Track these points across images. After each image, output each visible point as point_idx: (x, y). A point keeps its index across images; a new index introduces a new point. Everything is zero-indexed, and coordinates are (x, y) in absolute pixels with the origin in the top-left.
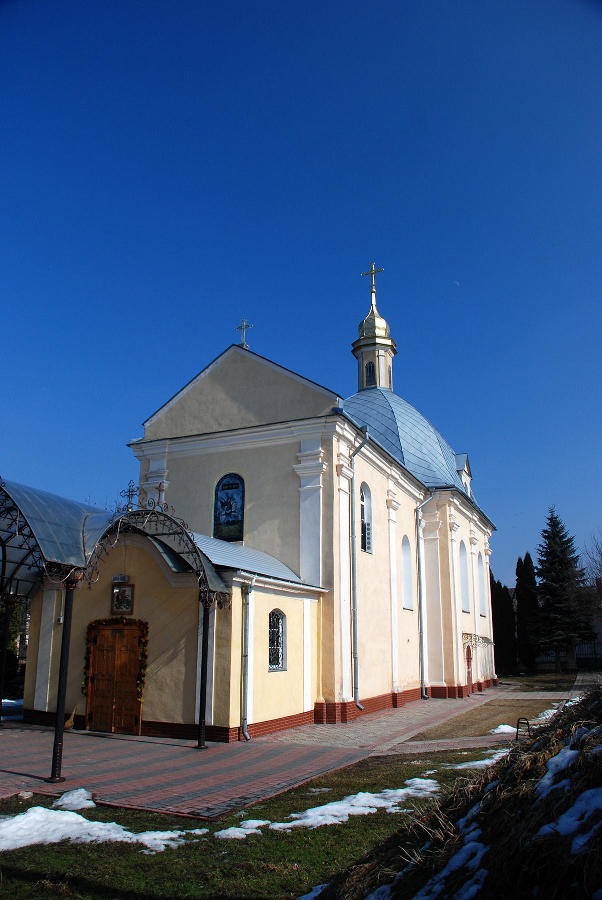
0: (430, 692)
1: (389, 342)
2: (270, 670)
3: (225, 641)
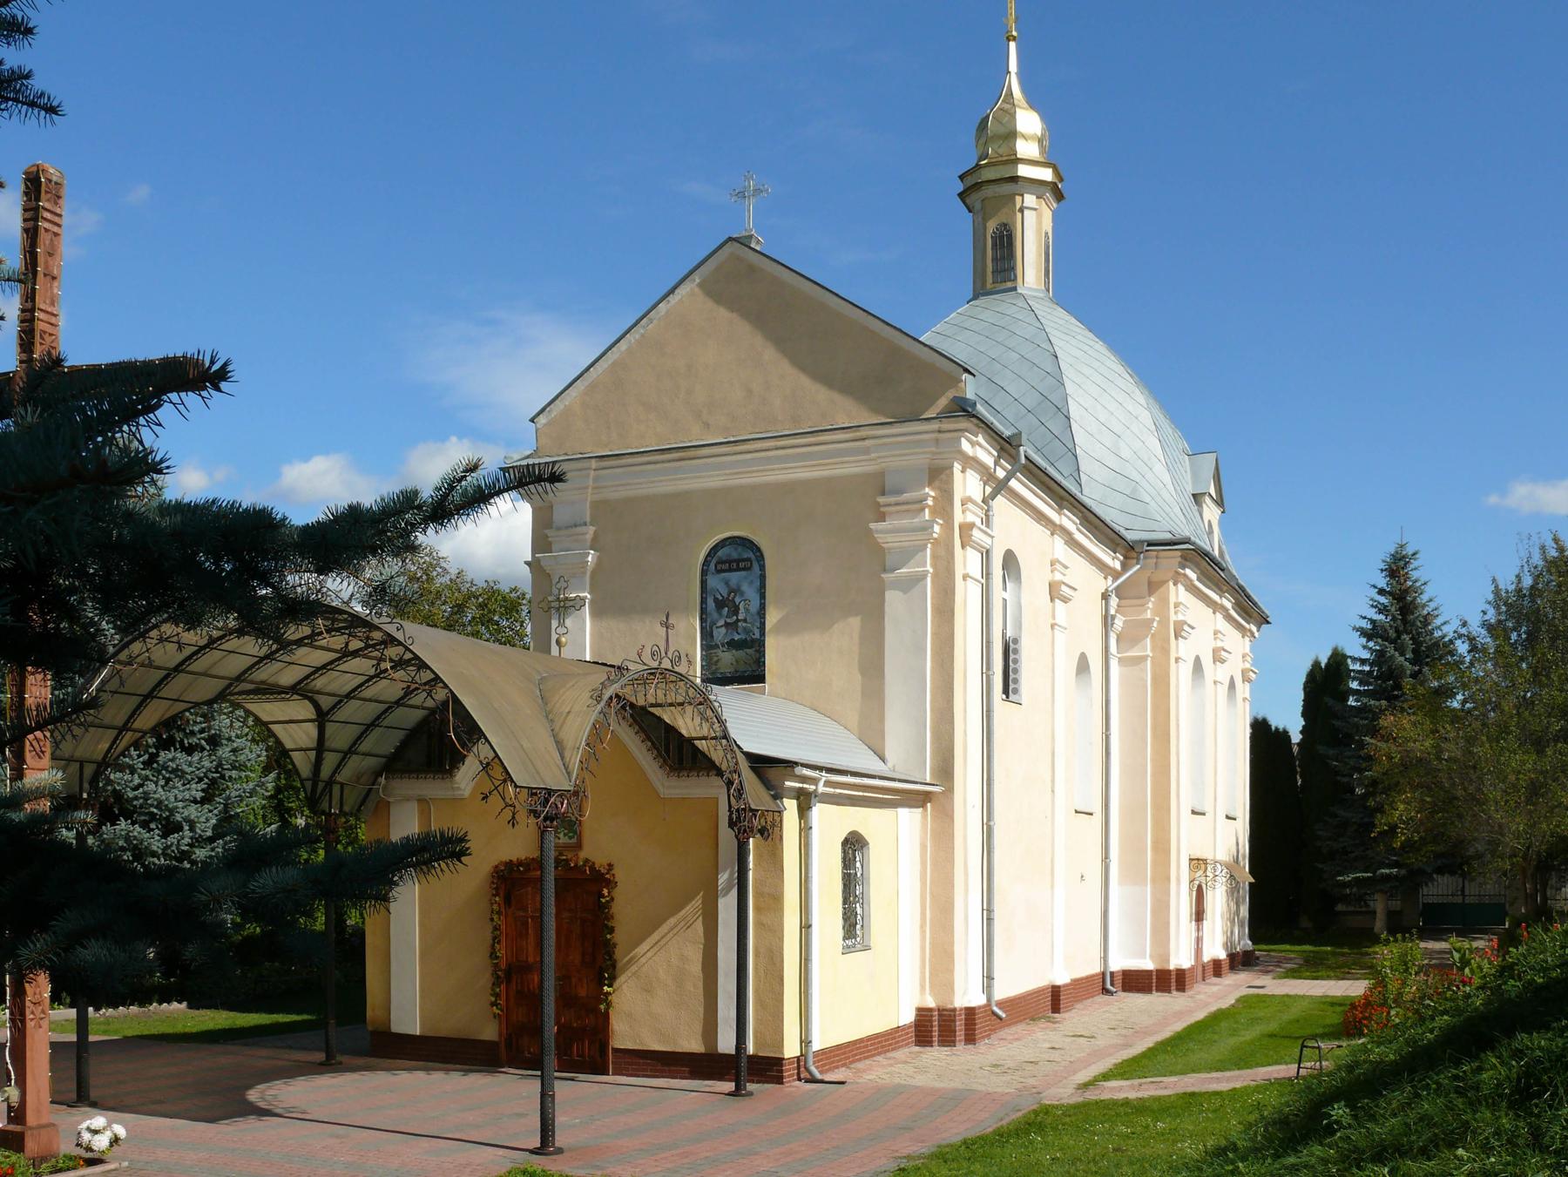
0: (1118, 982)
1: (1046, 174)
2: (847, 950)
3: (773, 901)
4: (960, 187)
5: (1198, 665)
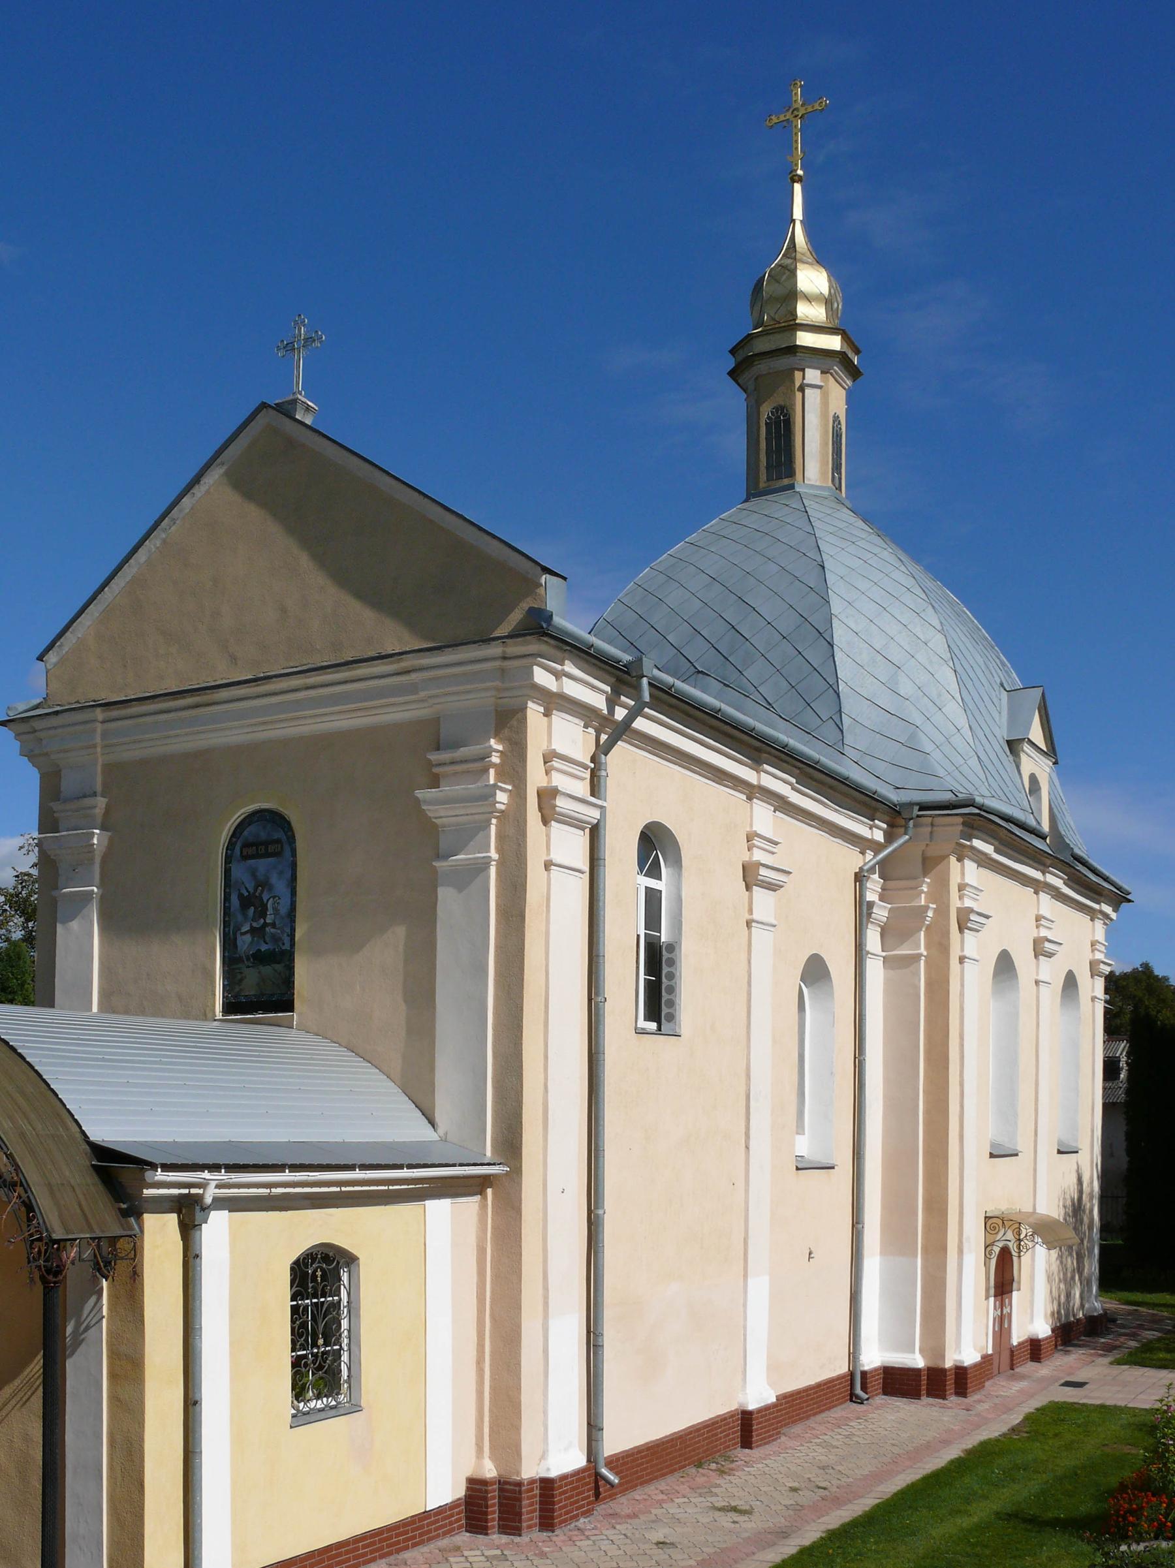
0: (876, 1383)
1: (834, 343)
2: (300, 1419)
4: (731, 363)
5: (1005, 965)
